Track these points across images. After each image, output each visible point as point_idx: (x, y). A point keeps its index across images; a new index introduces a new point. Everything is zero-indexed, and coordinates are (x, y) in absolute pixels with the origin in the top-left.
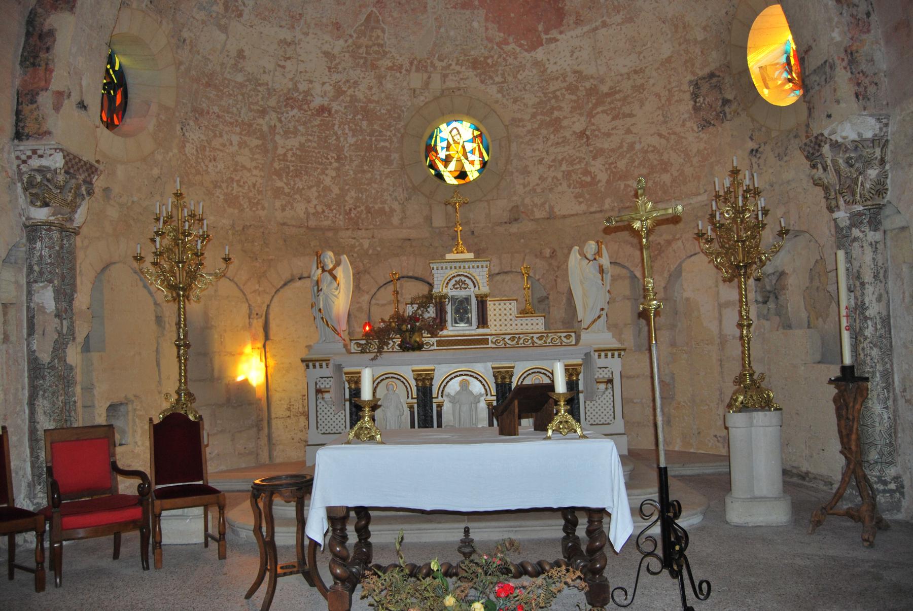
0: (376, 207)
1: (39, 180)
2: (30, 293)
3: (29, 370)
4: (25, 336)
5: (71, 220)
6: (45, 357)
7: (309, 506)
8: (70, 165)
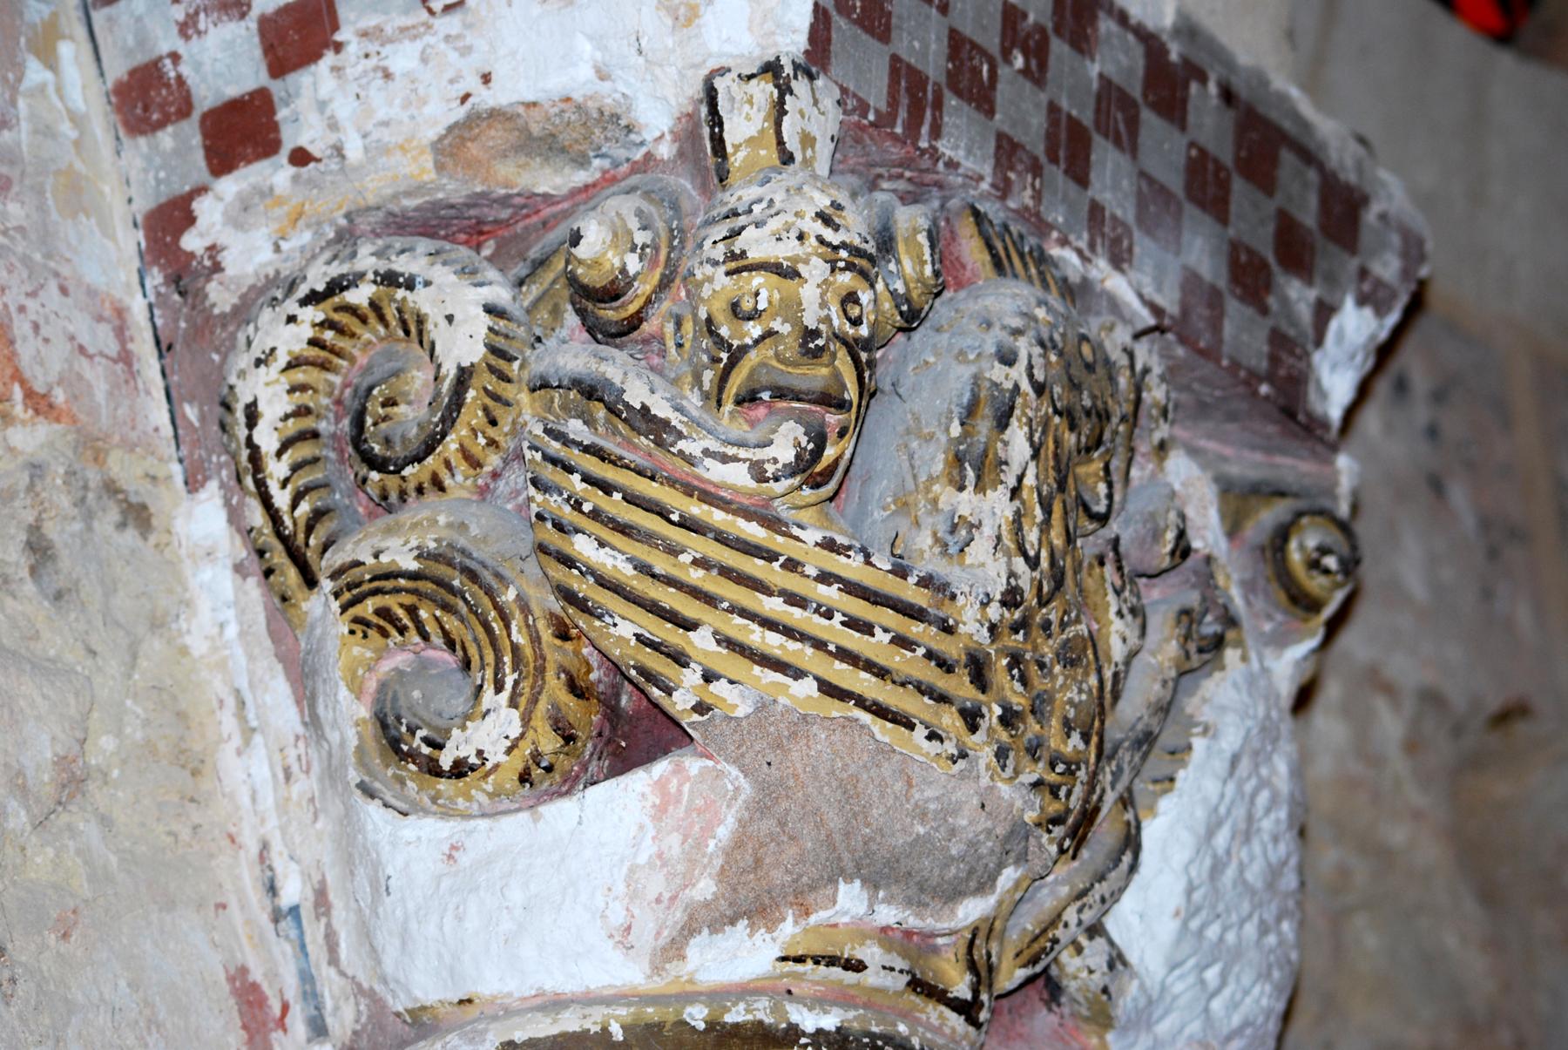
1: (463, 345)
7: (106, 115)
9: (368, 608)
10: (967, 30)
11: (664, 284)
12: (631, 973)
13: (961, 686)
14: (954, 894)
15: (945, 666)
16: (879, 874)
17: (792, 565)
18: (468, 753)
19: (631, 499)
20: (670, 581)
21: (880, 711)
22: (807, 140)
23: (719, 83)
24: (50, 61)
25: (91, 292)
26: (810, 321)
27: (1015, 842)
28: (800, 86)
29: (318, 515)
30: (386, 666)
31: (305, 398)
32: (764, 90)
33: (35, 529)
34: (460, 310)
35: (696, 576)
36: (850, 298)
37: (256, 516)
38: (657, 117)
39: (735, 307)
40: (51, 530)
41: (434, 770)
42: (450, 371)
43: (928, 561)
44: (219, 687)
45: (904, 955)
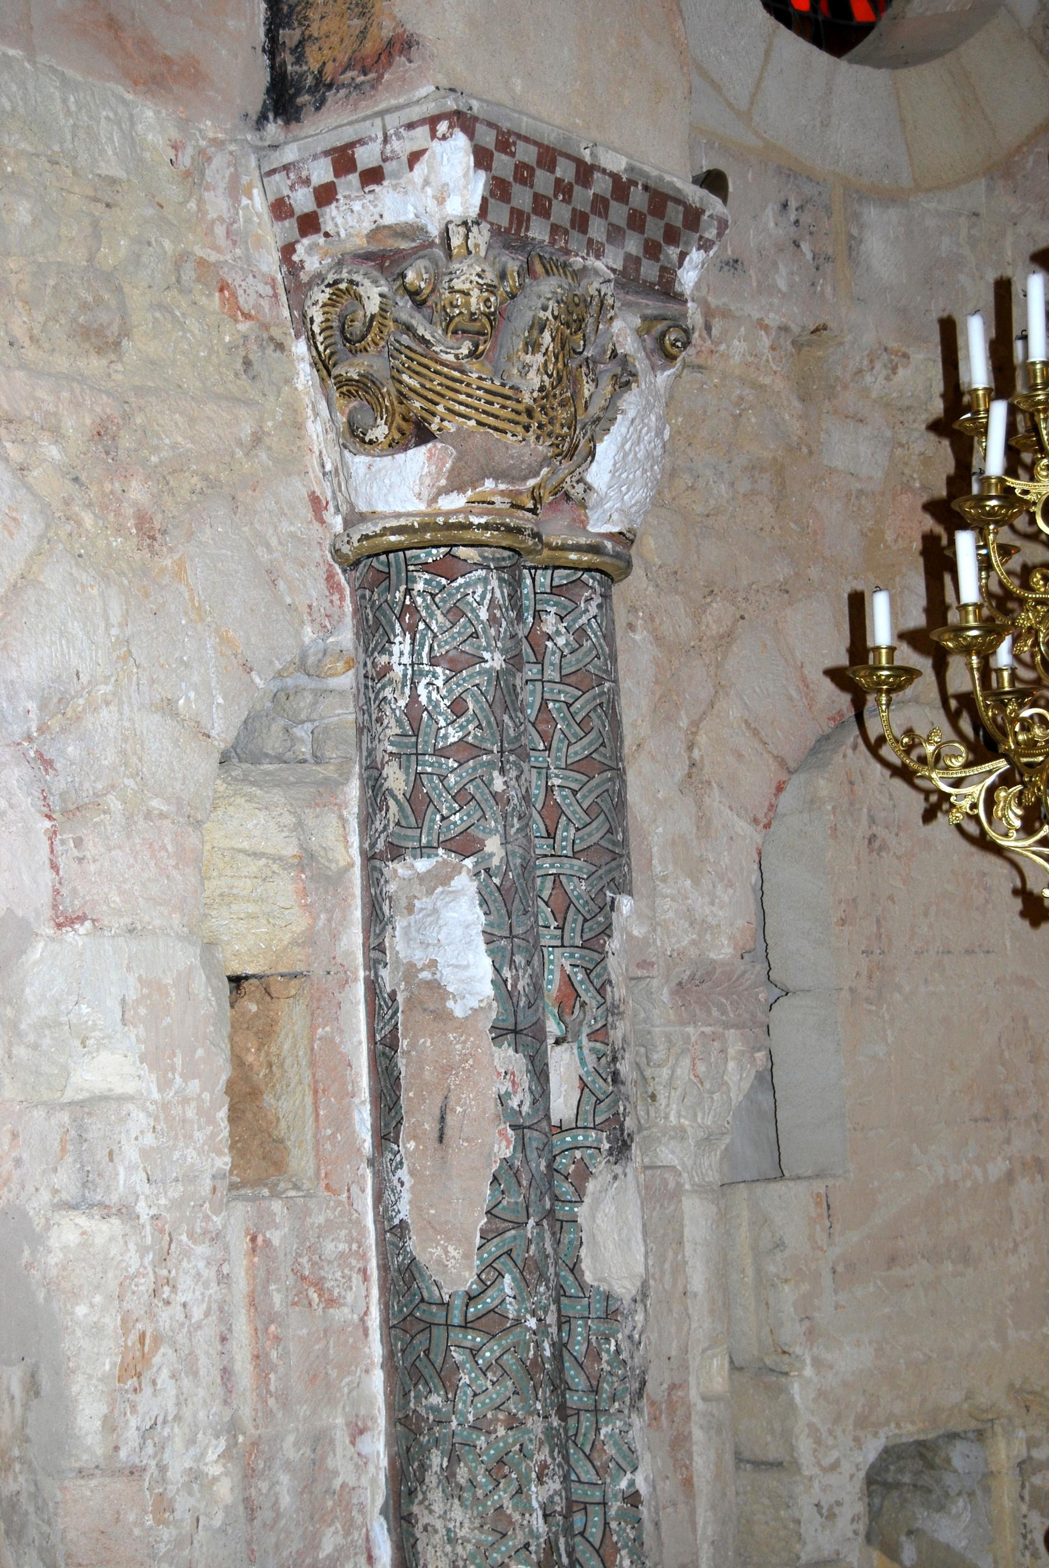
0: (107, 1367)
1: (373, 306)
2: (376, 918)
3: (388, 1327)
4: (367, 1146)
5: (569, 499)
6: (452, 1265)
8: (522, 198)
9: (345, 389)
10: (541, 191)
11: (433, 291)
12: (422, 507)
13: (524, 419)
14: (525, 478)
15: (518, 413)
16: (497, 477)
17: (468, 385)
18: (373, 437)
19: (419, 364)
20: (430, 390)
21: (496, 429)
22: (477, 246)
23: (450, 227)
24: (250, 197)
25: (263, 275)
26: (473, 310)
27: (546, 461)
28: (475, 229)
29: (332, 354)
30: (351, 405)
31: (329, 316)
32: (462, 230)
33: (246, 357)
34: (372, 295)
35: (439, 388)
36: (488, 300)
37: (315, 354)
38: (434, 231)
39: (451, 303)
40: (251, 356)
41: (363, 441)
42: (368, 314)
43: (516, 381)
44: (307, 400)
45: (509, 497)
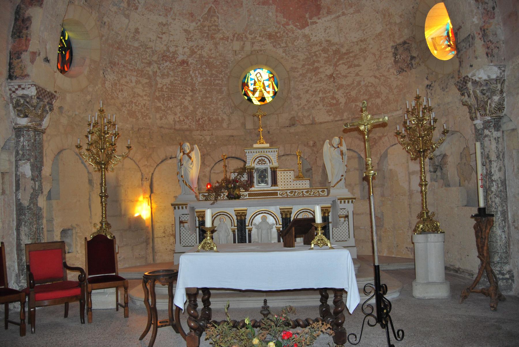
0: (214, 118)
1: (22, 102)
2: (17, 167)
3: (16, 210)
4: (14, 191)
5: (40, 125)
6: (26, 203)
8: (40, 94)
